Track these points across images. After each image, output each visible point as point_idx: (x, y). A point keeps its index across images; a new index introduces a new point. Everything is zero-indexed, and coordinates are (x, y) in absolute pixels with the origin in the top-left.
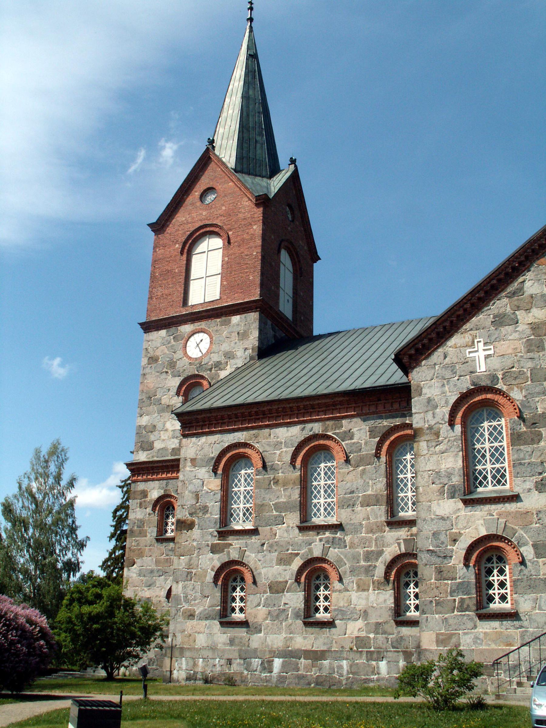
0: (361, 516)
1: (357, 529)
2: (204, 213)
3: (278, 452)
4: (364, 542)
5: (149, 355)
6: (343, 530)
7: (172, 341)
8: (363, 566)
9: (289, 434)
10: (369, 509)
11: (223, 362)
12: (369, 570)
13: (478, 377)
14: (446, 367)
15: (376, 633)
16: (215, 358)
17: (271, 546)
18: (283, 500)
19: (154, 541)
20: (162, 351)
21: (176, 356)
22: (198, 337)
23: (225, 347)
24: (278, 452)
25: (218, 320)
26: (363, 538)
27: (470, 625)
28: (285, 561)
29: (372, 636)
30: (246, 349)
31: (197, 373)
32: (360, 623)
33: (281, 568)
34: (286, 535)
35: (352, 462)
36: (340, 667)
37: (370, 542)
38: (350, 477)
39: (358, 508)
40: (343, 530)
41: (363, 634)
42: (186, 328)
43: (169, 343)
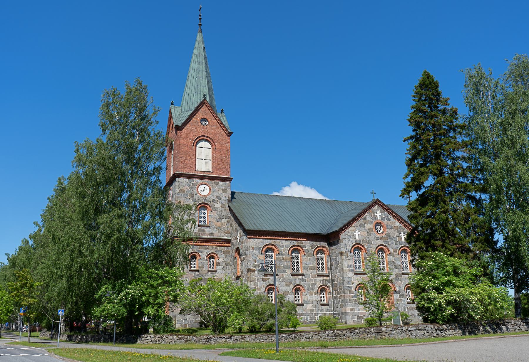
0: (310, 272)
1: (309, 276)
2: (203, 130)
3: (283, 249)
4: (311, 280)
5: (180, 189)
6: (304, 276)
7: (191, 185)
8: (311, 288)
9: (286, 243)
10: (312, 270)
11: (216, 200)
12: (313, 289)
13: (357, 240)
14: (349, 236)
15: (315, 308)
16: (213, 198)
17: (283, 280)
18: (286, 265)
19: (189, 271)
20: (187, 188)
21: (194, 192)
22: (203, 186)
23: (217, 194)
24: (283, 249)
25: (213, 181)
26: (310, 279)
27: (357, 306)
28: (288, 285)
29: (314, 309)
30: (226, 197)
31: (204, 202)
32: (311, 305)
33: (287, 287)
34: (287, 276)
35: (306, 255)
36: (307, 318)
37: (313, 281)
38: (306, 260)
39: (309, 270)
40: (304, 276)
41: (312, 308)
42: (199, 181)
43: (190, 186)
